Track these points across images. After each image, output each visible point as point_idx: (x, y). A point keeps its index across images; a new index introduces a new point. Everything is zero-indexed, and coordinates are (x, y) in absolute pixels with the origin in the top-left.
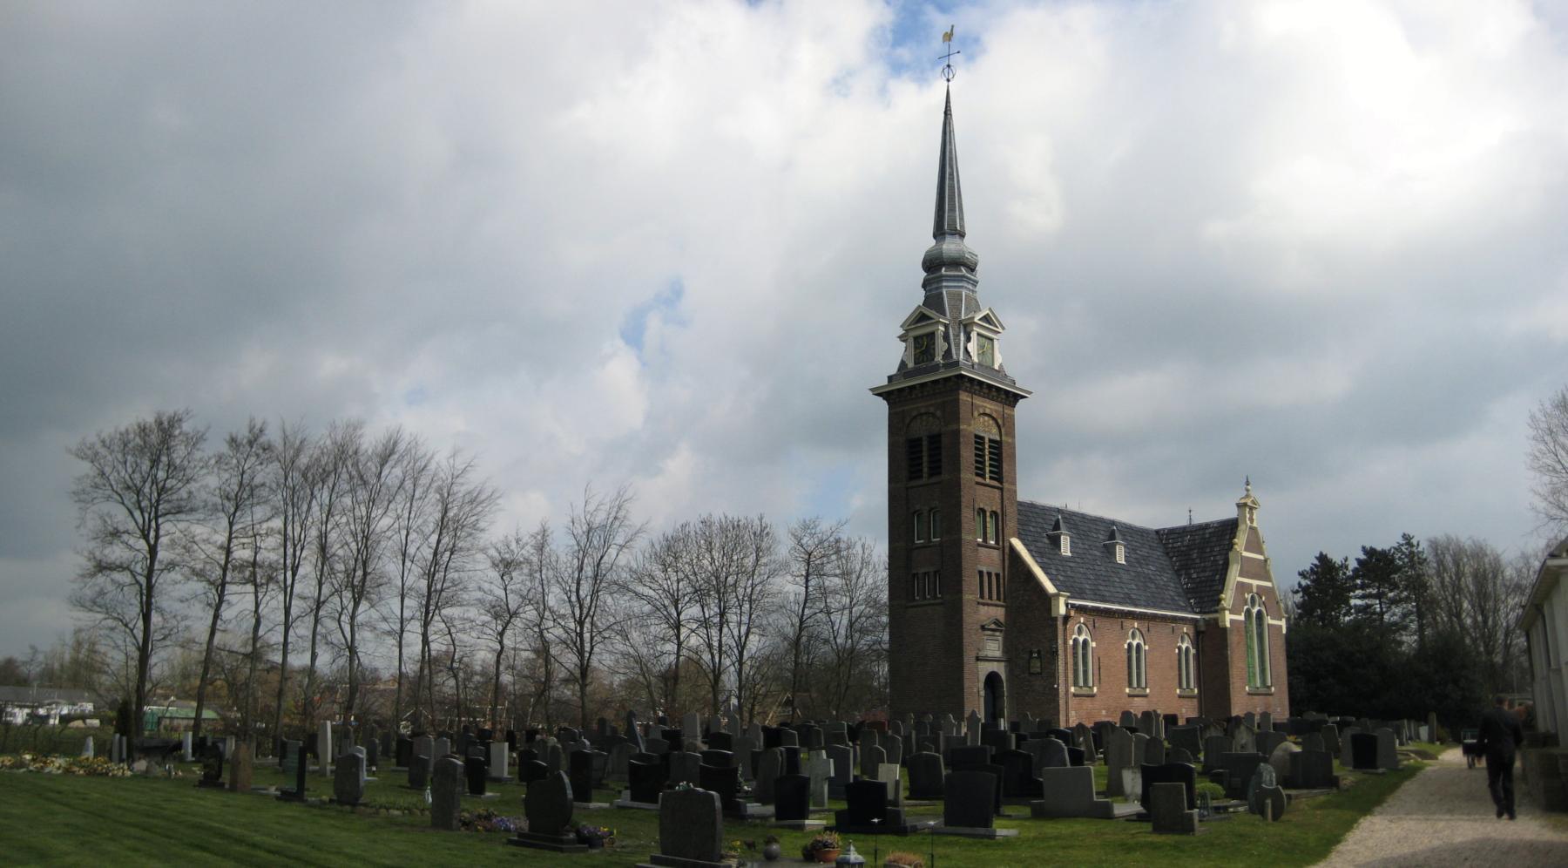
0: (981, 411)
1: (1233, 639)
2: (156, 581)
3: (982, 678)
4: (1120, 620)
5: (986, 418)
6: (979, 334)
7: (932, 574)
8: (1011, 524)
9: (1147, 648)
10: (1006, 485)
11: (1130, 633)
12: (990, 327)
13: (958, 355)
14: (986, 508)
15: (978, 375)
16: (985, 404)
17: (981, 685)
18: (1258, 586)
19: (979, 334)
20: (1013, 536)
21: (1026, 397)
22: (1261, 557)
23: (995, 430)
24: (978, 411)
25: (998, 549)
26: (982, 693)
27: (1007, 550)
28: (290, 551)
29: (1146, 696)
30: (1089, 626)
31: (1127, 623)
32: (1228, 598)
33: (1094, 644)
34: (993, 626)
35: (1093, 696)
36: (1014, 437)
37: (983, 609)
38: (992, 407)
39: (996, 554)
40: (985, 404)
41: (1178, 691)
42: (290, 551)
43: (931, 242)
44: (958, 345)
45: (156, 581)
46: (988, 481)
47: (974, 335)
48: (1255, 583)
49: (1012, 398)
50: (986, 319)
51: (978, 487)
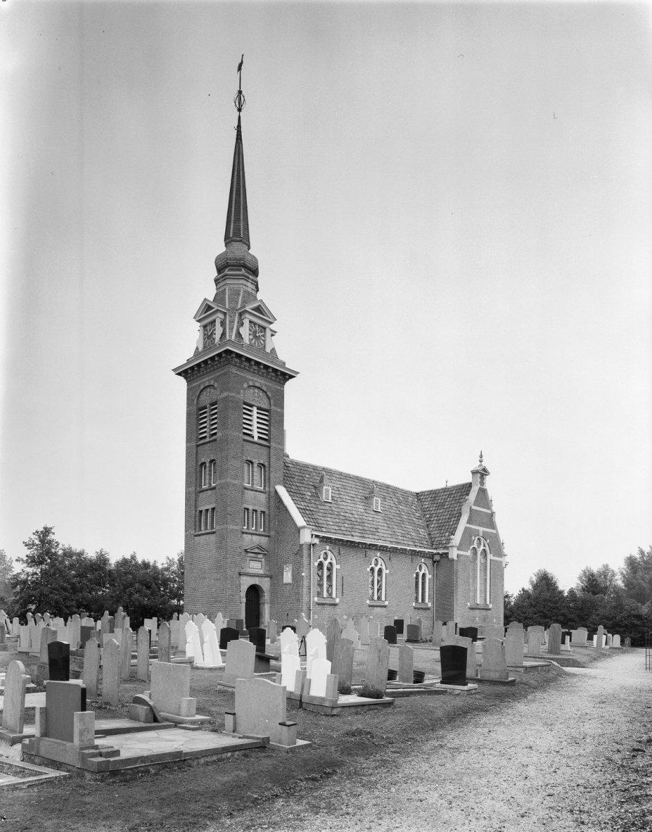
0: (251, 384)
1: (459, 568)
2: (496, 671)
3: (244, 588)
4: (364, 550)
5: (256, 390)
6: (251, 322)
7: (210, 510)
8: (276, 474)
9: (388, 572)
10: (273, 444)
11: (373, 560)
12: (265, 318)
13: (230, 336)
14: (253, 461)
15: (262, 359)
16: (255, 379)
17: (243, 594)
18: (484, 532)
19: (251, 322)
20: (279, 484)
21: (294, 377)
22: (489, 512)
23: (266, 400)
24: (248, 383)
25: (265, 493)
26: (244, 600)
27: (272, 494)
28: (648, 660)
29: (385, 607)
30: (335, 553)
31: (370, 553)
32: (457, 539)
33: (338, 567)
34: (257, 551)
35: (335, 605)
36: (282, 407)
37: (247, 538)
38: (262, 382)
39: (263, 497)
40: (255, 379)
41: (414, 604)
42: (648, 660)
43: (223, 249)
44: (231, 329)
45: (496, 671)
46: (256, 439)
47: (246, 322)
48: (481, 529)
49: (284, 376)
50: (258, 309)
51: (245, 443)
